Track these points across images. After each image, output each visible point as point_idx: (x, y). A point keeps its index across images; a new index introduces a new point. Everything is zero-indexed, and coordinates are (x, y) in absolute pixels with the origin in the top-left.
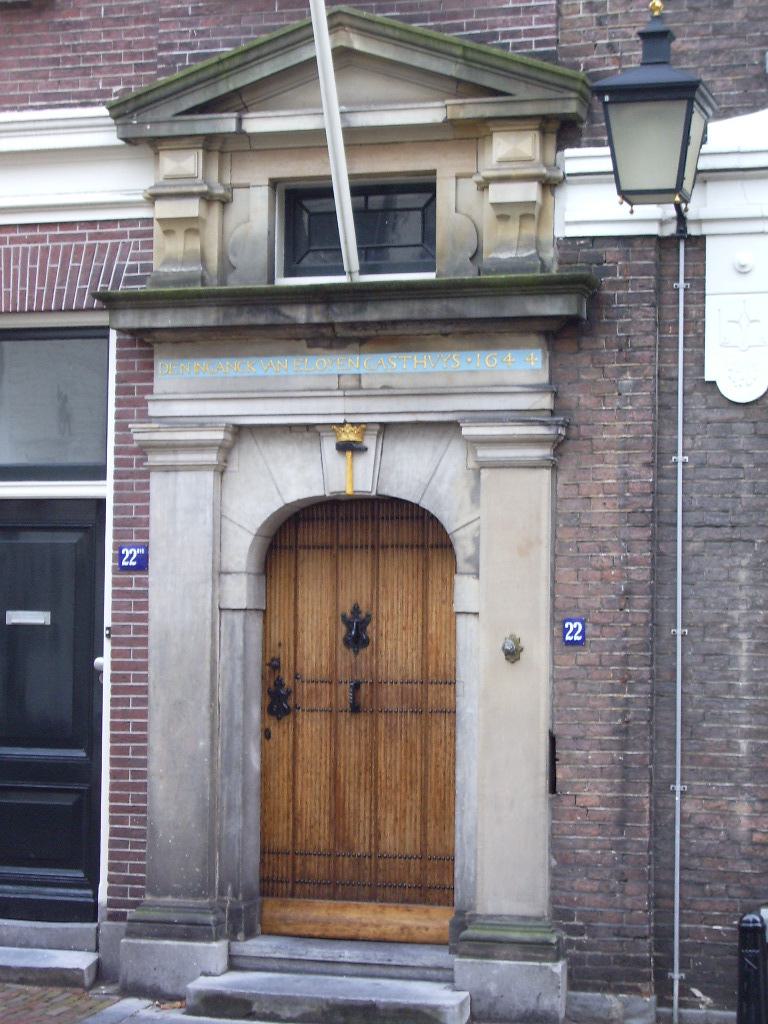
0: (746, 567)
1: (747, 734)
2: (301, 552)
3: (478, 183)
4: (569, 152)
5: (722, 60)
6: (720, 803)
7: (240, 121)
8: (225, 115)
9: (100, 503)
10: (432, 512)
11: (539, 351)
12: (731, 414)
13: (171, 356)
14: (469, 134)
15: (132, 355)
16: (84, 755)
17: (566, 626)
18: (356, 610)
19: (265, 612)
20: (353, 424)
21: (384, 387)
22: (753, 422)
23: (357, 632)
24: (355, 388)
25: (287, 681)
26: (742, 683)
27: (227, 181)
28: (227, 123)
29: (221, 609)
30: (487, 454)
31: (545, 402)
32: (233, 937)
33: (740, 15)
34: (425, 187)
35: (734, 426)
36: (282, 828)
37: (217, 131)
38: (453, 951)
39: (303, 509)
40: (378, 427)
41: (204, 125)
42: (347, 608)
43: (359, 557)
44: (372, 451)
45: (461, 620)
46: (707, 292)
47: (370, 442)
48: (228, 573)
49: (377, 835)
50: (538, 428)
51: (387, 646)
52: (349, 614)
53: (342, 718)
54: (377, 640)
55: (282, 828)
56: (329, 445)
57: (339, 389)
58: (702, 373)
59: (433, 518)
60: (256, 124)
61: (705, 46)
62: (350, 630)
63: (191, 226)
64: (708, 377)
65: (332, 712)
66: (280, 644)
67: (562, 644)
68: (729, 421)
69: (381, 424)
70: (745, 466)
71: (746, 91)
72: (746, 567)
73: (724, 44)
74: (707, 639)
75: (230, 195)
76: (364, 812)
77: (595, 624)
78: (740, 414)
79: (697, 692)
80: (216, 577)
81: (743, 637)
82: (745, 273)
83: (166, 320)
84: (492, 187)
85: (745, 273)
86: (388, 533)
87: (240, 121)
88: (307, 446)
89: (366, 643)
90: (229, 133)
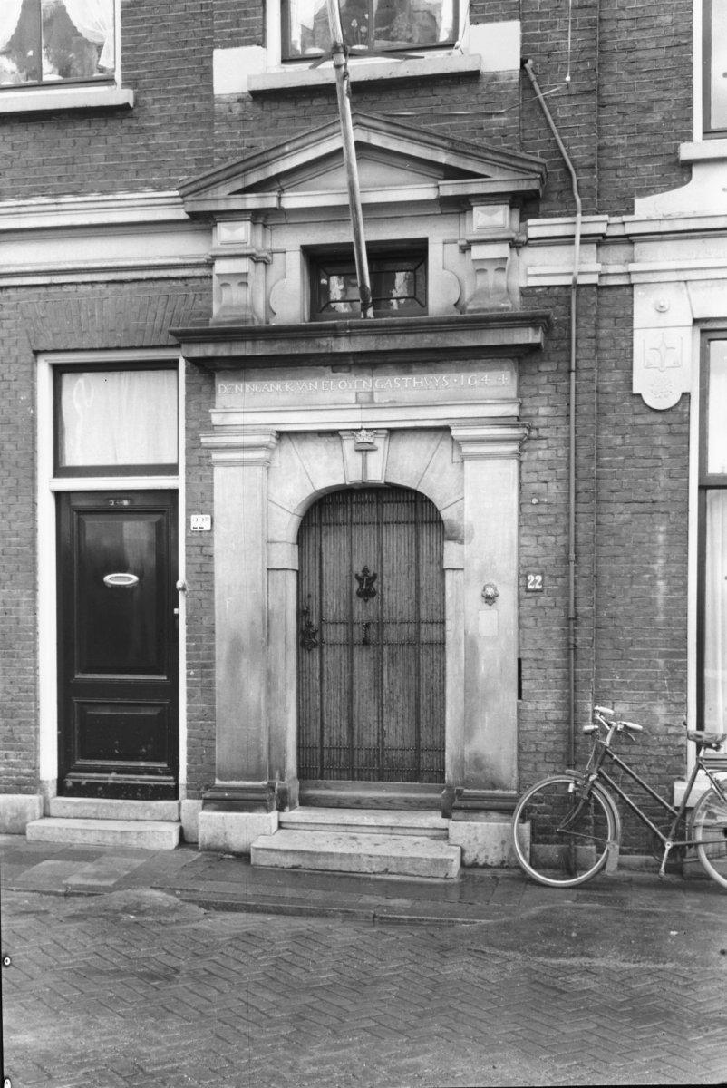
0: (663, 533)
1: (662, 655)
2: (324, 528)
3: (461, 247)
4: (530, 222)
5: (644, 152)
6: (643, 706)
7: (280, 198)
8: (270, 194)
9: (174, 492)
10: (429, 497)
11: (508, 373)
12: (651, 418)
13: (225, 378)
14: (459, 206)
15: (193, 384)
16: (165, 678)
17: (529, 578)
18: (366, 570)
19: (298, 572)
20: (367, 429)
21: (390, 402)
22: (669, 425)
23: (367, 586)
24: (369, 403)
25: (315, 622)
26: (661, 618)
27: (269, 247)
28: (271, 201)
29: (268, 569)
30: (468, 449)
31: (513, 410)
32: (281, 809)
33: (658, 117)
34: (416, 253)
35: (654, 427)
36: (315, 730)
37: (266, 206)
38: (446, 815)
39: (325, 496)
40: (386, 432)
41: (252, 202)
42: (358, 569)
43: (368, 530)
44: (381, 450)
45: (448, 575)
46: (635, 327)
47: (380, 443)
48: (273, 542)
49: (382, 733)
50: (510, 429)
51: (389, 597)
52: (360, 574)
53: (356, 650)
54: (382, 592)
55: (315, 730)
56: (349, 445)
57: (356, 403)
58: (631, 388)
59: (430, 501)
60: (293, 200)
61: (632, 142)
62: (361, 585)
63: (242, 280)
64: (635, 391)
65: (350, 644)
66: (309, 596)
67: (524, 593)
68: (651, 424)
69: (389, 429)
70: (663, 457)
71: (663, 175)
72: (663, 533)
73: (646, 140)
74: (634, 586)
75: (270, 258)
76: (373, 718)
77: (551, 576)
78: (659, 418)
79: (626, 625)
80: (265, 545)
81: (661, 584)
82: (664, 312)
83: (223, 351)
84: (474, 248)
85: (664, 312)
86: (389, 512)
87: (280, 198)
88: (331, 447)
89: (374, 594)
90: (271, 209)
